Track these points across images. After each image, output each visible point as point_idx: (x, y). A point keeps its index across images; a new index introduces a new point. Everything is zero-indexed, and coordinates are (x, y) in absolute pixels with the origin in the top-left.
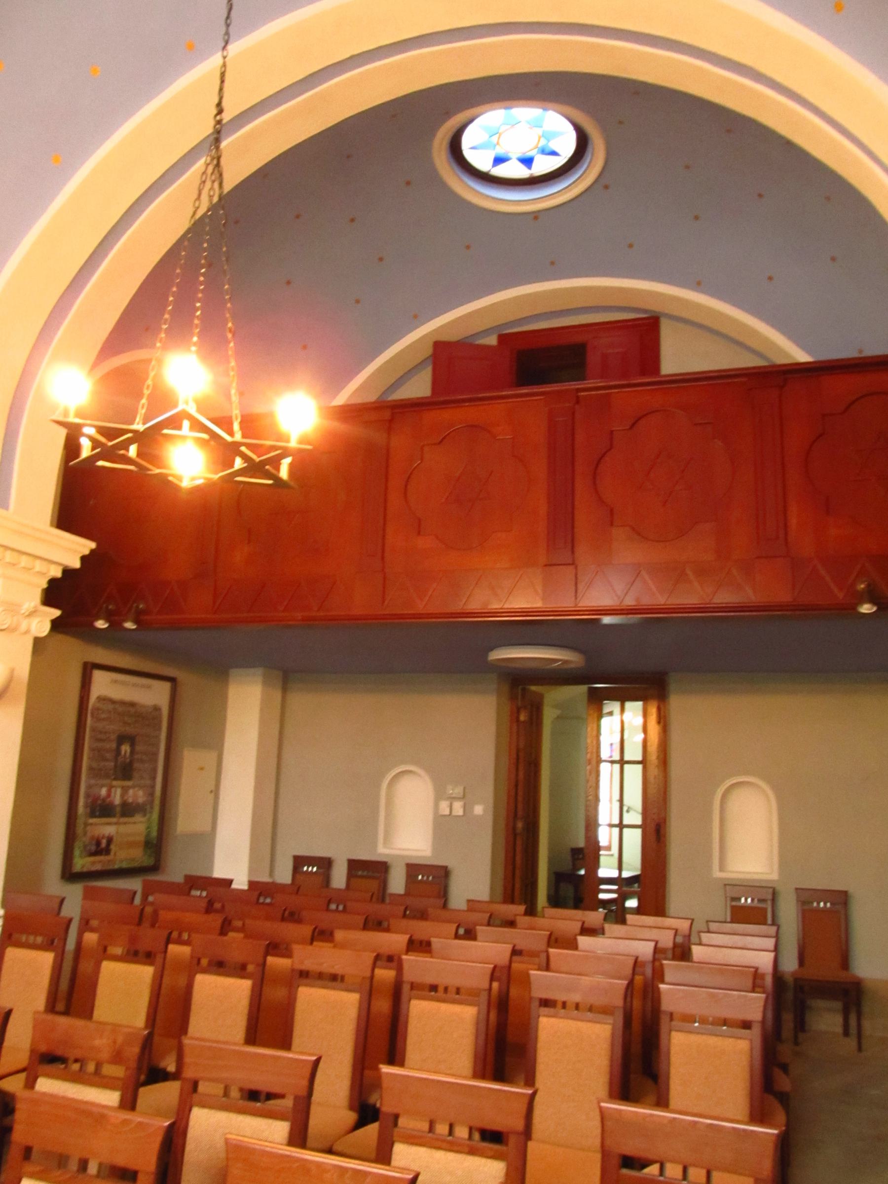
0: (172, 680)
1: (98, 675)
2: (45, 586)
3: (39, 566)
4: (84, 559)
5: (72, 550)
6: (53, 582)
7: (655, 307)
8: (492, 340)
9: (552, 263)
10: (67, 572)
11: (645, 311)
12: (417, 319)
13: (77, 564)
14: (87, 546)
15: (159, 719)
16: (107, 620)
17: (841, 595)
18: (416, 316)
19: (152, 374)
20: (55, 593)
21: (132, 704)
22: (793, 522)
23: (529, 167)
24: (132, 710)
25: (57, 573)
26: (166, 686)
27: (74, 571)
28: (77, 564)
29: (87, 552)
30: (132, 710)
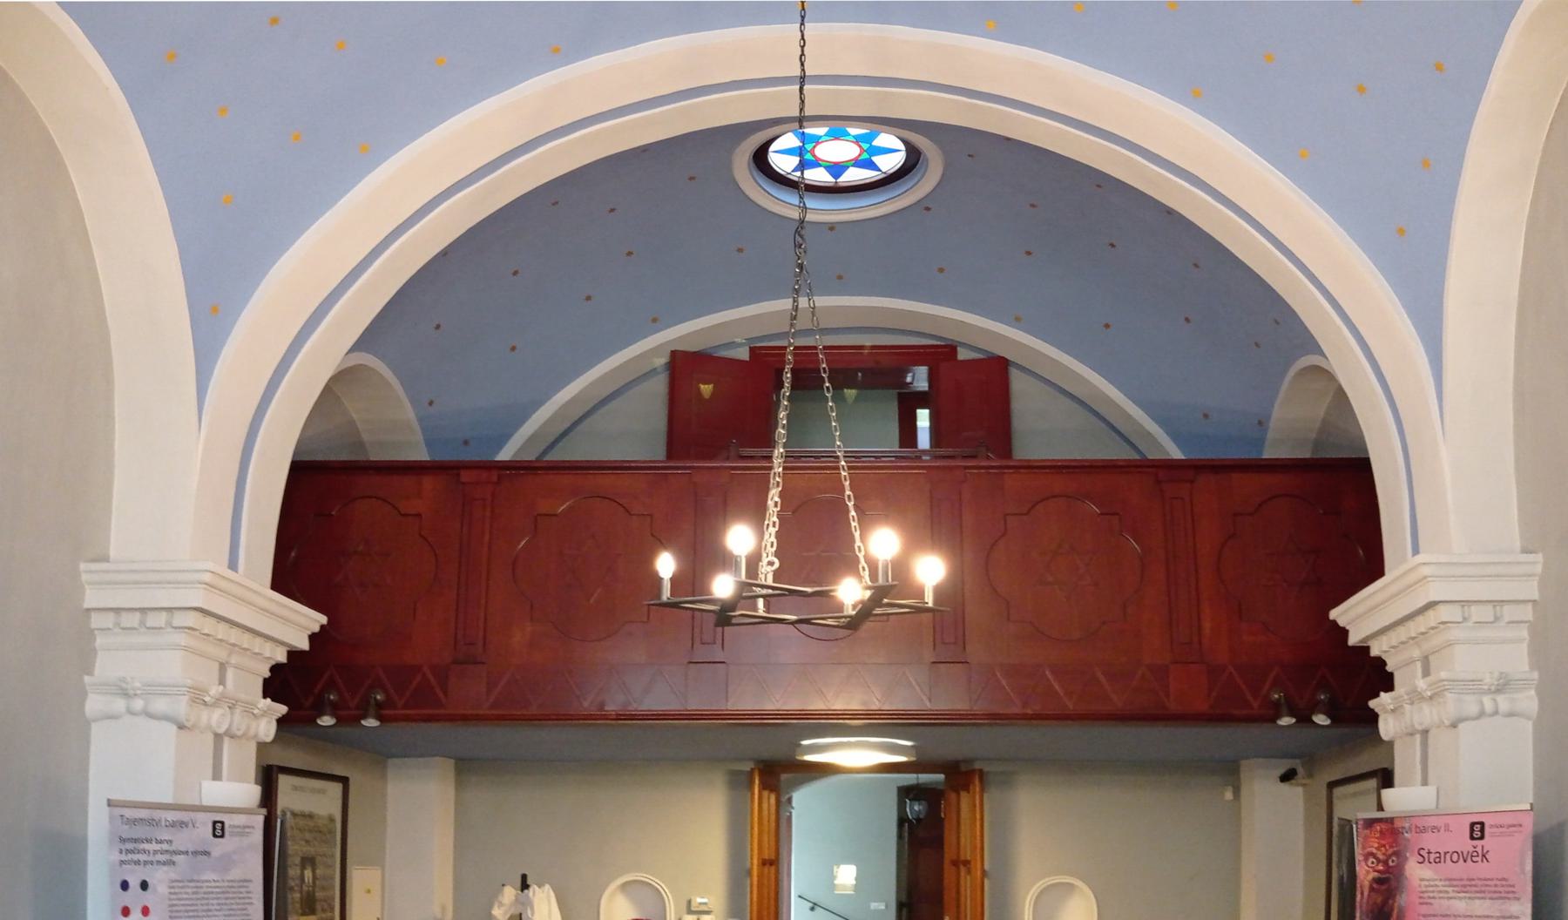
0: (345, 781)
1: (284, 783)
2: (267, 674)
3: (257, 645)
4: (313, 638)
5: (298, 624)
6: (276, 669)
7: (952, 335)
8: (743, 354)
9: (840, 277)
10: (293, 654)
11: (941, 338)
12: (656, 323)
13: (305, 645)
14: (315, 620)
15: (332, 832)
16: (333, 715)
17: (1255, 705)
18: (654, 320)
19: (861, 556)
20: (277, 684)
21: (311, 816)
22: (1207, 626)
23: (836, 176)
24: (311, 824)
25: (282, 657)
26: (336, 788)
27: (302, 652)
28: (305, 645)
29: (317, 629)
30: (311, 824)
